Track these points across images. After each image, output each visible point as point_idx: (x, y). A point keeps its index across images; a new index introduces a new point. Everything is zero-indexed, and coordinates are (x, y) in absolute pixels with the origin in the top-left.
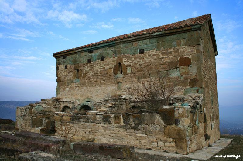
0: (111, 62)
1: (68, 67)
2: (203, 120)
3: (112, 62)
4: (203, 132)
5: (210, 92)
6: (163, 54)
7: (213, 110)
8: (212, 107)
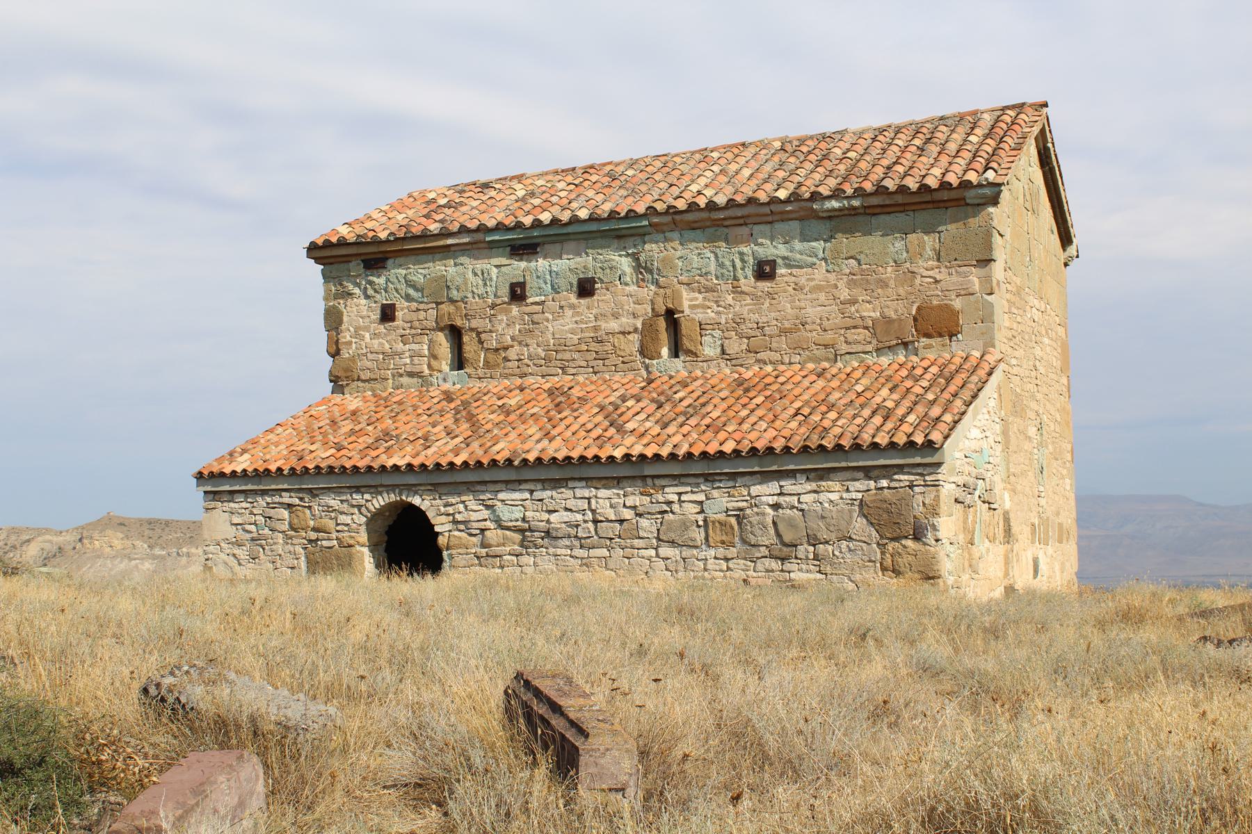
0: (626, 302)
1: (399, 314)
2: (911, 264)
3: (630, 306)
4: (1001, 574)
5: (1032, 431)
6: (851, 284)
7: (1043, 502)
8: (1042, 489)
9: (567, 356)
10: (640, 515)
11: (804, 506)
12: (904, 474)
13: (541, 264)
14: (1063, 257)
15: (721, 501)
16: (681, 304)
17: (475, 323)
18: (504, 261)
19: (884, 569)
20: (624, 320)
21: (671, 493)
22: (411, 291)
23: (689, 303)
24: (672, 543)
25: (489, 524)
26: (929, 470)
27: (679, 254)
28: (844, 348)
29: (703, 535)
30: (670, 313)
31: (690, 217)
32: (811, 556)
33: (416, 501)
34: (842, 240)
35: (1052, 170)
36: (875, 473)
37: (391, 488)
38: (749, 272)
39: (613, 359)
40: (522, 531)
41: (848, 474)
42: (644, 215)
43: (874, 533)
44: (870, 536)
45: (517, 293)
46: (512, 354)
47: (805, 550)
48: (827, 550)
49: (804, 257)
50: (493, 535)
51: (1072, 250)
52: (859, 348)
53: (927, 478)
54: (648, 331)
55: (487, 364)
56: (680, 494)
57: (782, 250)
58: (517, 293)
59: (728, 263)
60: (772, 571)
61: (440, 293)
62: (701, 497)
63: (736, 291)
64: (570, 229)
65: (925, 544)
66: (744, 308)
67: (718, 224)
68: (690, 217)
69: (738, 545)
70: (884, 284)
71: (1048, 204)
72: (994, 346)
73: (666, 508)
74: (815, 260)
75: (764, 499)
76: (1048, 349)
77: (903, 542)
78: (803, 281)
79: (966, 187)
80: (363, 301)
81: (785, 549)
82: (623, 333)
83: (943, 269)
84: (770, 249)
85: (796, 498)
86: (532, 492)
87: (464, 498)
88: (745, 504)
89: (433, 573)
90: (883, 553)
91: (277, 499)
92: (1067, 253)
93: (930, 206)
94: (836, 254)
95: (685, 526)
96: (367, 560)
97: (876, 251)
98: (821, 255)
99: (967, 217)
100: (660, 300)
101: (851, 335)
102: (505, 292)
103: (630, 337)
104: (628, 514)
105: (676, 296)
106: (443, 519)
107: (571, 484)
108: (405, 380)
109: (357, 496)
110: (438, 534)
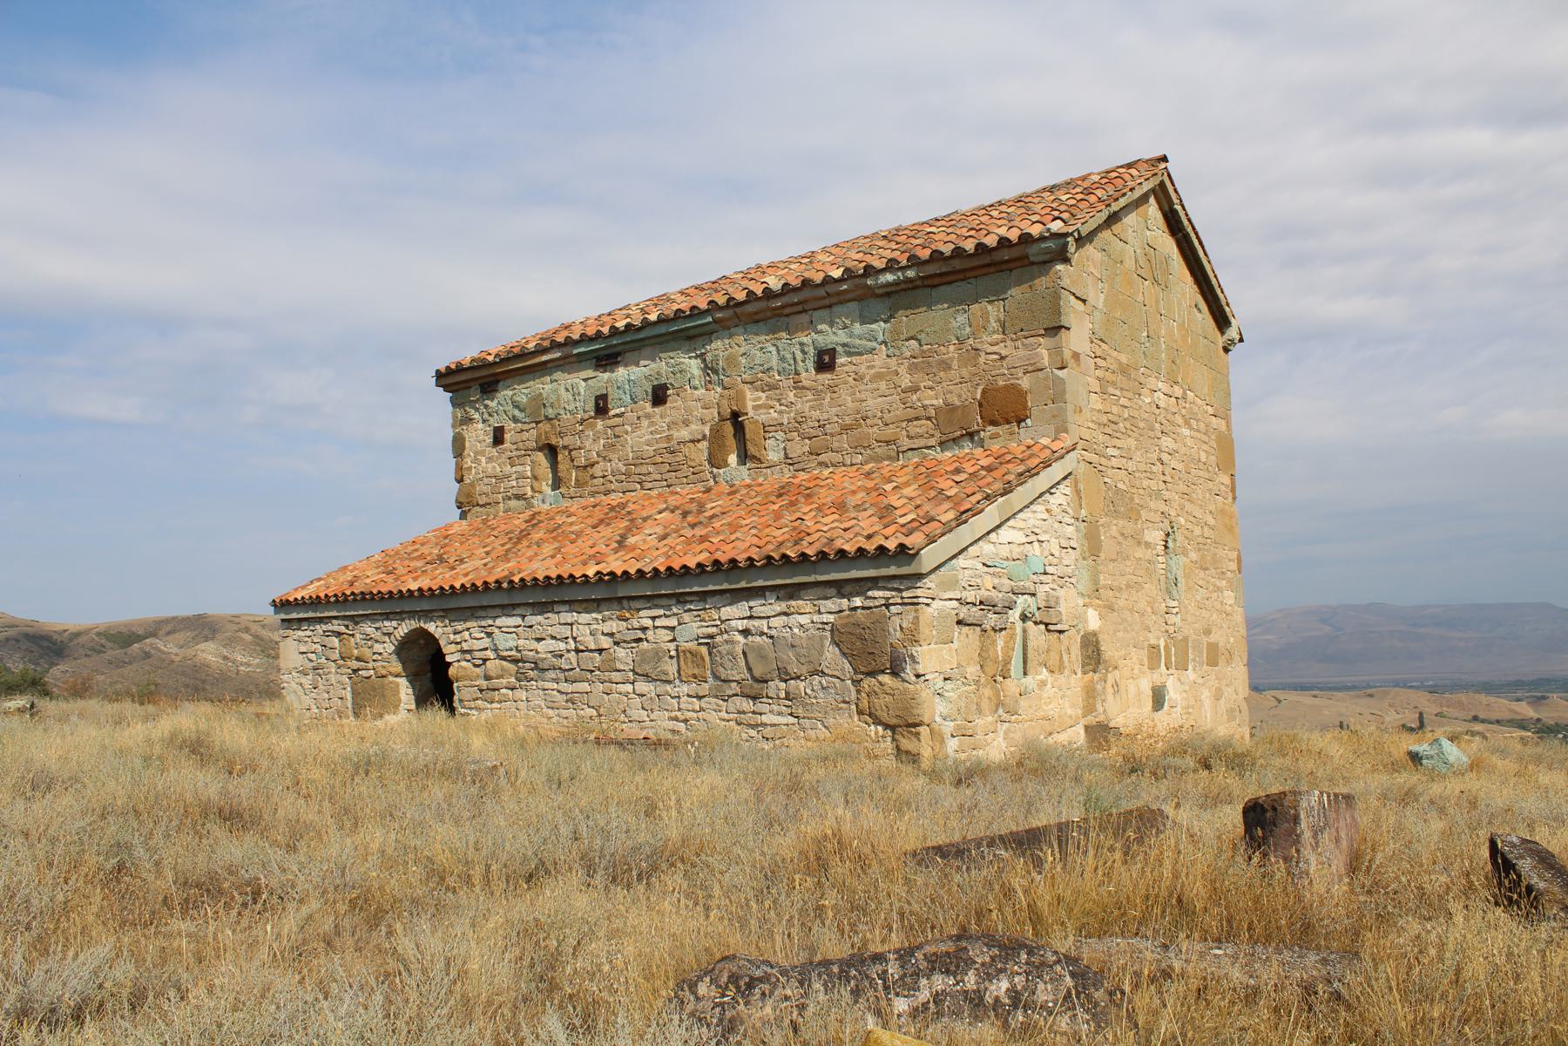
0: (696, 407)
1: (507, 436)
3: (699, 412)
6: (913, 369)
9: (643, 469)
10: (617, 644)
11: (773, 632)
12: (879, 589)
13: (621, 372)
14: (1221, 341)
15: (691, 625)
16: (745, 406)
17: (566, 441)
18: (590, 373)
19: (860, 712)
20: (693, 427)
21: (644, 618)
22: (517, 412)
23: (753, 402)
24: (647, 677)
27: (742, 350)
28: (906, 443)
29: (675, 667)
30: (735, 415)
31: (750, 308)
32: (783, 695)
33: (431, 627)
34: (902, 317)
35: (1187, 237)
36: (848, 589)
37: (412, 614)
38: (811, 365)
39: (686, 471)
40: (515, 661)
42: (707, 311)
43: (847, 666)
44: (843, 669)
46: (597, 471)
47: (777, 687)
48: (798, 688)
49: (864, 342)
50: (493, 666)
51: (1232, 333)
53: (905, 594)
54: (716, 438)
55: (579, 484)
56: (653, 618)
57: (842, 337)
59: (789, 356)
60: (744, 712)
61: (537, 412)
62: (673, 622)
63: (798, 385)
64: (642, 335)
65: (904, 680)
66: (804, 405)
67: (777, 313)
68: (750, 308)
69: (710, 680)
70: (945, 365)
72: (1066, 431)
73: (640, 634)
74: (874, 344)
75: (733, 623)
76: (1189, 442)
77: (880, 678)
78: (863, 369)
79: (1026, 242)
80: (480, 426)
81: (756, 685)
82: (693, 441)
83: (1009, 343)
84: (829, 335)
85: (764, 622)
86: (523, 617)
87: (469, 624)
88: (714, 630)
90: (858, 692)
91: (329, 627)
92: (1226, 337)
93: (992, 269)
94: (896, 332)
95: (658, 655)
96: (405, 691)
97: (937, 328)
98: (881, 338)
99: (1033, 278)
100: (725, 402)
101: (915, 428)
102: (591, 405)
103: (699, 445)
104: (606, 642)
105: (740, 397)
106: (453, 648)
107: (557, 608)
108: (513, 503)
109: (387, 623)
110: (450, 664)
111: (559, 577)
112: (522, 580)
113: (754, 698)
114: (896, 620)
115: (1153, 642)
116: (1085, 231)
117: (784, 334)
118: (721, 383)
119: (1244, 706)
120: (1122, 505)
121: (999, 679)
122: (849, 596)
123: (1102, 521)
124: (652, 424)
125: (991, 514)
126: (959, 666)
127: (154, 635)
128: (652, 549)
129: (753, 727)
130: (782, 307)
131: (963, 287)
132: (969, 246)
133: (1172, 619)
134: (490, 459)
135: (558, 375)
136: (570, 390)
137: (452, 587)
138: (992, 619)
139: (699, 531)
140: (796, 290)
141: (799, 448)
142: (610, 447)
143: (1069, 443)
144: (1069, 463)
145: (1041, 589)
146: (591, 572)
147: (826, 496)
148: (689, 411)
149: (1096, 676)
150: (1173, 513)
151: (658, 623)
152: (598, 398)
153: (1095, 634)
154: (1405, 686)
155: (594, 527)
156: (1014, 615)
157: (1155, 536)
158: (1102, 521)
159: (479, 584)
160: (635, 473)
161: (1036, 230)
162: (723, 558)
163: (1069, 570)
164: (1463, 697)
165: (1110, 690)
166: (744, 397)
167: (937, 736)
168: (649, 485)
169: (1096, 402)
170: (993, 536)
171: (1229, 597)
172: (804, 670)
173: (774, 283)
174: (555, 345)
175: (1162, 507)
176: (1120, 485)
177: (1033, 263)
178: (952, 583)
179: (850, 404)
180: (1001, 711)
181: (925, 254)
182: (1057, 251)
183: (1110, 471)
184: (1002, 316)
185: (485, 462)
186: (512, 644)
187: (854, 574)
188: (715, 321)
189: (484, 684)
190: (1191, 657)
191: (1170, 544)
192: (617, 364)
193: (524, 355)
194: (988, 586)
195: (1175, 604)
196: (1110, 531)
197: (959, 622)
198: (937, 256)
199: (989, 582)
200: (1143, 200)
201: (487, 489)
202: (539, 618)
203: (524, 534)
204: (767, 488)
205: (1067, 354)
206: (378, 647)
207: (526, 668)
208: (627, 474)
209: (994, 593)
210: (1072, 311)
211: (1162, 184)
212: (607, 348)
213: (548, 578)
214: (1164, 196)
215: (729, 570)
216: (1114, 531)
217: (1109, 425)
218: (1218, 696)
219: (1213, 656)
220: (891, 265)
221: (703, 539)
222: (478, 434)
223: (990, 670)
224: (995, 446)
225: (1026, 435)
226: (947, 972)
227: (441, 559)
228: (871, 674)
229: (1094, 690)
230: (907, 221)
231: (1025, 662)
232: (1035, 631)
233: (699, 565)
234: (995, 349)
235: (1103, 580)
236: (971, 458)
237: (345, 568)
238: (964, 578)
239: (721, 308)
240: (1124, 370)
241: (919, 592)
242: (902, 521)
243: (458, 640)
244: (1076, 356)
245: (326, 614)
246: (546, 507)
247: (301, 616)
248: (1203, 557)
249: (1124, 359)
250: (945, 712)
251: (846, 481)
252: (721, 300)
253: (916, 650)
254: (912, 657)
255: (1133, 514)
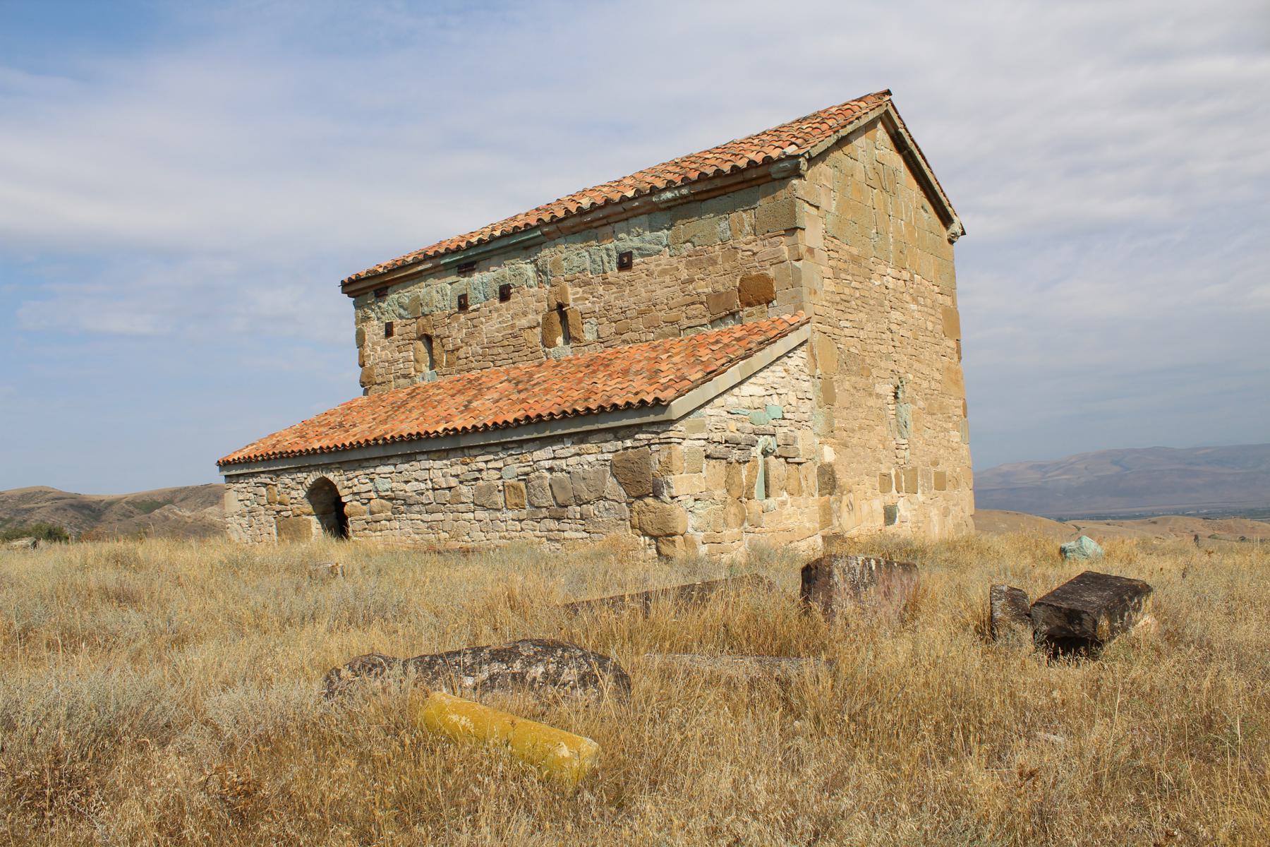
0: (532, 301)
1: (395, 330)
3: (534, 305)
6: (689, 265)
9: (495, 351)
10: (461, 482)
11: (570, 469)
13: (476, 277)
14: (946, 234)
15: (512, 466)
18: (454, 278)
19: (633, 527)
21: (480, 462)
22: (402, 311)
23: (572, 295)
25: (373, 495)
26: (663, 427)
27: (564, 256)
28: (685, 323)
30: (560, 306)
31: (568, 223)
32: (578, 516)
33: (331, 476)
34: (680, 226)
36: (621, 434)
37: (317, 467)
38: (614, 265)
39: (526, 351)
40: (391, 499)
41: (601, 436)
42: (537, 227)
43: (623, 492)
45: (463, 304)
46: (461, 353)
47: (574, 510)
50: (376, 503)
51: (955, 228)
52: (697, 322)
53: (661, 436)
54: (547, 325)
55: (449, 364)
56: (486, 462)
57: (636, 242)
58: (463, 304)
59: (598, 259)
61: (416, 310)
62: (500, 464)
63: (605, 282)
64: (490, 247)
66: (610, 296)
67: (589, 226)
68: (568, 223)
70: (713, 262)
71: (914, 182)
72: (802, 309)
76: (917, 315)
78: (652, 267)
80: (376, 322)
83: (759, 242)
84: (627, 241)
85: (563, 461)
87: (357, 473)
88: (529, 469)
89: (292, 540)
90: (631, 511)
91: (259, 480)
93: (745, 185)
95: (490, 490)
97: (706, 233)
98: (665, 242)
99: (775, 191)
100: (552, 296)
101: (693, 311)
104: (453, 482)
105: (563, 292)
106: (346, 491)
107: (392, 461)
108: (402, 381)
110: (345, 504)
111: (418, 434)
112: (392, 437)
113: (558, 519)
114: (656, 456)
115: (884, 471)
116: (814, 152)
117: (594, 243)
118: (549, 282)
119: (971, 521)
120: (854, 365)
121: (744, 500)
122: (622, 439)
123: (835, 378)
124: (500, 316)
125: (733, 374)
126: (708, 489)
127: (170, 502)
128: (486, 411)
129: (558, 541)
130: (592, 221)
131: (724, 201)
132: (727, 168)
133: (902, 453)
134: (384, 348)
135: (431, 281)
136: (439, 292)
137: (344, 445)
138: (736, 454)
139: (523, 396)
140: (601, 207)
141: (608, 330)
142: (470, 334)
143: (804, 318)
144: (804, 333)
145: (780, 431)
146: (440, 429)
147: (618, 365)
148: (527, 304)
149: (832, 498)
150: (902, 371)
151: (490, 465)
152: (460, 297)
153: (830, 465)
154: (1183, 514)
155: (453, 396)
156: (756, 451)
157: (886, 389)
158: (835, 378)
159: (362, 441)
160: (489, 355)
161: (775, 154)
162: (532, 414)
163: (806, 416)
164: (1231, 522)
165: (845, 509)
166: (566, 292)
167: (690, 543)
168: (499, 363)
169: (829, 285)
170: (736, 391)
171: (955, 436)
172: (592, 496)
173: (585, 203)
174: (427, 258)
175: (892, 366)
176: (852, 350)
177: (775, 180)
178: (701, 427)
179: (644, 294)
180: (746, 524)
181: (694, 176)
182: (791, 169)
183: (843, 340)
184: (753, 221)
185: (380, 350)
186: (388, 486)
187: (625, 422)
188: (543, 234)
189: (369, 517)
190: (920, 482)
191: (900, 395)
192: (473, 270)
193: (404, 266)
194: (732, 429)
195: (905, 441)
196: (844, 386)
197: (707, 457)
198: (703, 177)
199: (733, 426)
200: (871, 125)
201: (382, 371)
202: (407, 466)
203: (404, 403)
204: (582, 361)
205: (802, 249)
206: (294, 493)
207: (399, 503)
208: (484, 355)
209: (738, 434)
210: (806, 215)
211: (887, 112)
212: (466, 258)
213: (410, 434)
214: (889, 121)
215: (536, 423)
216: (847, 385)
217: (842, 303)
218: (946, 513)
219: (941, 482)
220: (670, 185)
221: (524, 401)
222: (374, 329)
223: (736, 493)
224: (749, 323)
225: (772, 312)
226: (503, 661)
227: (341, 425)
228: (640, 497)
229: (830, 508)
230: (695, 151)
231: (767, 487)
232: (776, 465)
233: (516, 420)
234: (749, 247)
235: (836, 423)
236: (730, 331)
237: (273, 435)
238: (710, 423)
239: (547, 224)
240: (855, 260)
241: (671, 434)
242: (663, 381)
243: (346, 483)
244: (811, 250)
245: (257, 470)
246: (425, 383)
247: (239, 472)
248: (930, 405)
249: (855, 251)
250: (696, 525)
251: (638, 354)
252: (547, 218)
253: (671, 478)
254: (667, 483)
255: (865, 371)
